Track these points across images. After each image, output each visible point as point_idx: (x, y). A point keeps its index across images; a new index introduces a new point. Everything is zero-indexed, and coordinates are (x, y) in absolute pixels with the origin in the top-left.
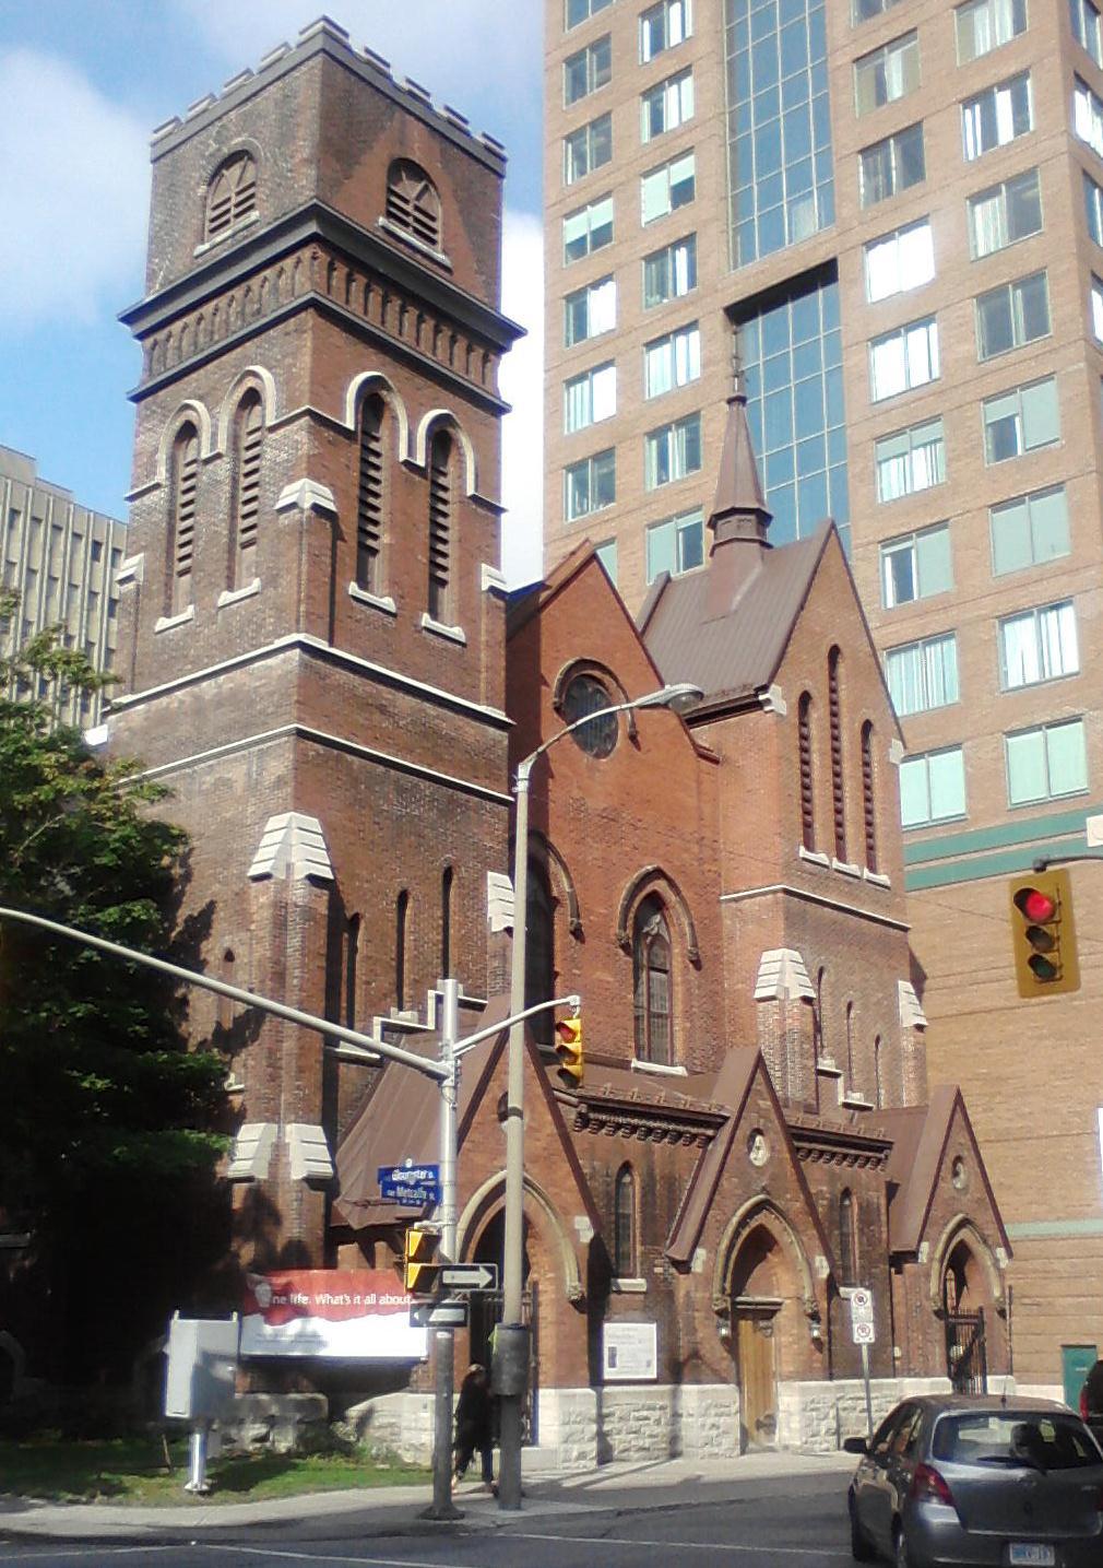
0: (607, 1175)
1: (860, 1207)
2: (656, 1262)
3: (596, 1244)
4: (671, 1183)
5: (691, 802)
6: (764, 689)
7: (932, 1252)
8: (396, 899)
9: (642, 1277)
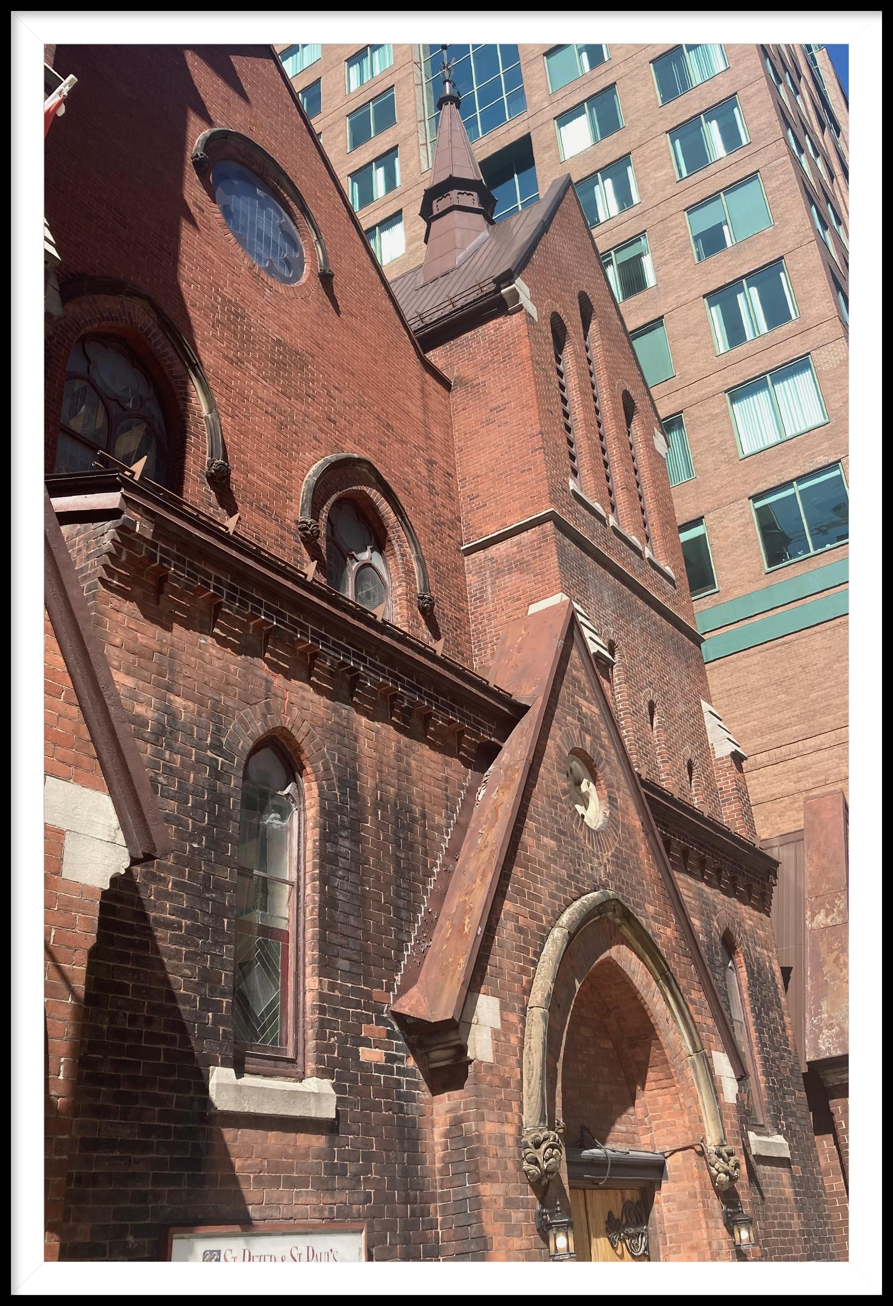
0: (216, 747)
2: (365, 1030)
3: (121, 904)
4: (404, 822)
6: (507, 277)
9: (322, 1074)
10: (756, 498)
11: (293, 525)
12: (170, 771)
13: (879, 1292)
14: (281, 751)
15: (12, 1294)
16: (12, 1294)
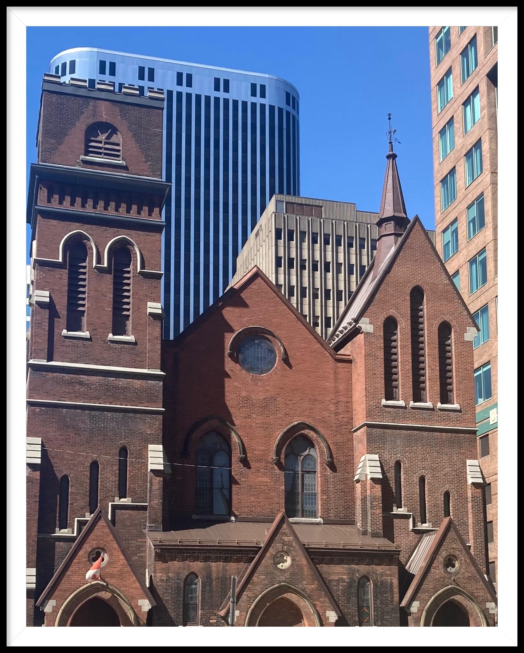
1: (375, 585)
5: (329, 385)
7: (420, 610)
8: (89, 465)
11: (271, 460)
12: (169, 586)
14: (194, 575)
15: (8, 645)
16: (8, 645)
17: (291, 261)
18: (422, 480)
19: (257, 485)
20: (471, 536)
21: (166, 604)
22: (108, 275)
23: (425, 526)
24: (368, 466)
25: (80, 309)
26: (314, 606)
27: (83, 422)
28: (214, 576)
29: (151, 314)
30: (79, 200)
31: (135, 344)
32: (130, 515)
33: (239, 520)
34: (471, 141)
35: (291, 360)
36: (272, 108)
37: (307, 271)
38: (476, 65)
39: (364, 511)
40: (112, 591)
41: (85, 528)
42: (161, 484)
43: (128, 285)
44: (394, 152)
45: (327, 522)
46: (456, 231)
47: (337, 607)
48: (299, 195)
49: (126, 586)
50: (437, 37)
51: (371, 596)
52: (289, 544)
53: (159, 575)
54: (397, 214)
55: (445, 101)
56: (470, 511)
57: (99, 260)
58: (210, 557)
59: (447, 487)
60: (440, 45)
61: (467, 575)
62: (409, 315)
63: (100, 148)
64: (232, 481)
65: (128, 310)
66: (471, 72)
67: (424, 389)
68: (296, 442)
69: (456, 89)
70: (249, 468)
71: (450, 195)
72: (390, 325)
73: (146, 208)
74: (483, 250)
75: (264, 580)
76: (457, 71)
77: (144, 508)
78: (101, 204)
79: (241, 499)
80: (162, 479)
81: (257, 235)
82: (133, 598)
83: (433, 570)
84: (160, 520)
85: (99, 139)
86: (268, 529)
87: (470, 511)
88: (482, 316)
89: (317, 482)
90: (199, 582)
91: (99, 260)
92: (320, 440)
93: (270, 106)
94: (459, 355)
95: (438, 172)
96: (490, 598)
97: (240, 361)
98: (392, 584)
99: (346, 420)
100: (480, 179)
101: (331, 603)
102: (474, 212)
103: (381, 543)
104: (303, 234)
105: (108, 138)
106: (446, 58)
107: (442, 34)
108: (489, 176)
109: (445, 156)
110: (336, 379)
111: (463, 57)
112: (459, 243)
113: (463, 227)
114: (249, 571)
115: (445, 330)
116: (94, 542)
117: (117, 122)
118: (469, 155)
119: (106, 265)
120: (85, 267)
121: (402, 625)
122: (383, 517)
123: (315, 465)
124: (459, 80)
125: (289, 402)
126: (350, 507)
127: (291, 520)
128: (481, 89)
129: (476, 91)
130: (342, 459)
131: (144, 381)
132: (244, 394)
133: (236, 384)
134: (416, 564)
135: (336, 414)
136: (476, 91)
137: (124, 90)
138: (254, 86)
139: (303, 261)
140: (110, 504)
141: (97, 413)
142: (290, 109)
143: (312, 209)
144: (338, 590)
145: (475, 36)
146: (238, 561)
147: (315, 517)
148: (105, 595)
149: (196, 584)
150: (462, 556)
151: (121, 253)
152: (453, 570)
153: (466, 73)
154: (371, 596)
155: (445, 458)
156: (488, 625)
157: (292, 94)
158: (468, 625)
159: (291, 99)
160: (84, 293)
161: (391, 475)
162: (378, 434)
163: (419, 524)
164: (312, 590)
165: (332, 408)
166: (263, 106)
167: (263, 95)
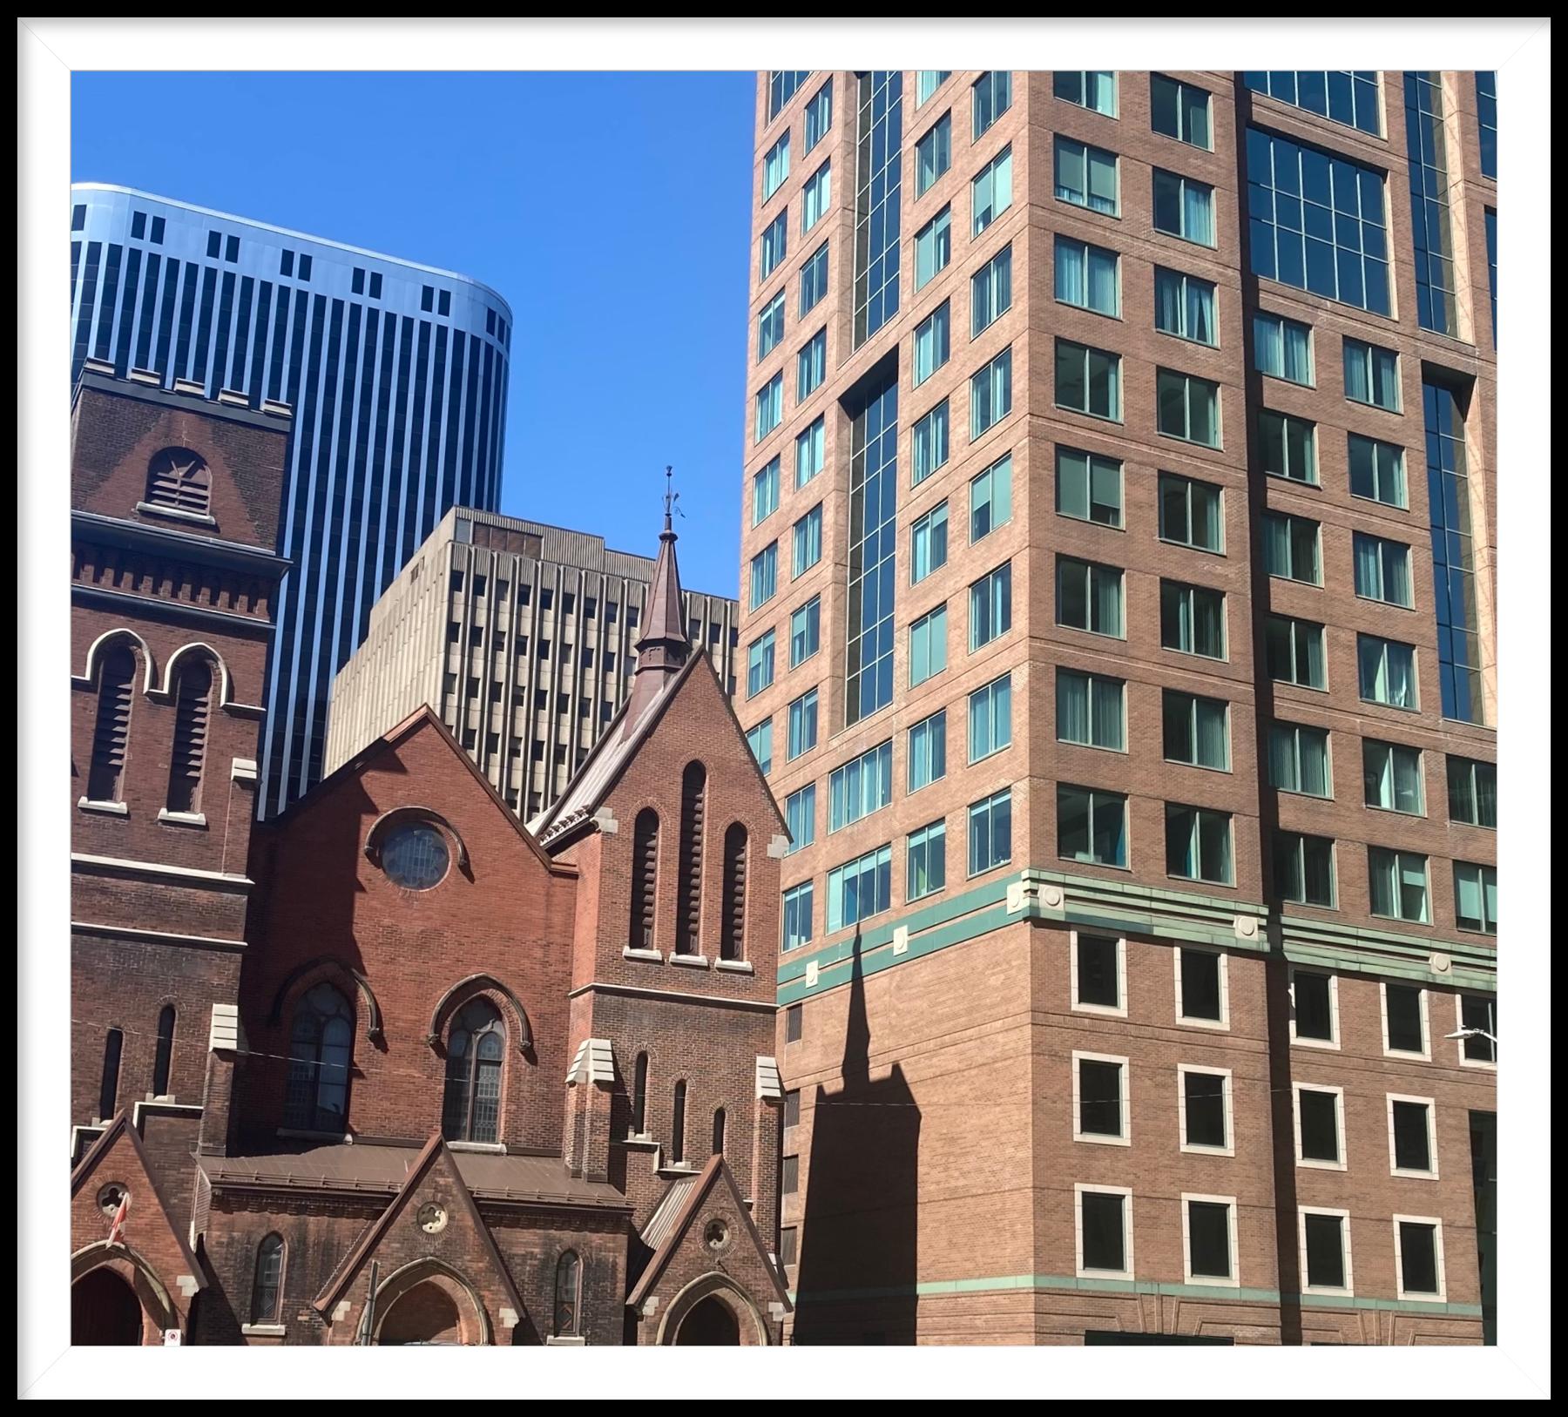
1: (587, 1266)
5: (538, 914)
7: (659, 1312)
10: (972, 806)
13: (1548, 1397)
15: (20, 1397)
16: (20, 1397)
17: (476, 632)
18: (681, 1086)
19: (395, 1080)
20: (755, 1187)
21: (225, 1286)
22: (168, 708)
23: (680, 1167)
24: (590, 1059)
25: (114, 762)
26: (481, 1299)
27: (102, 958)
28: (311, 1239)
29: (237, 779)
30: (128, 577)
31: (206, 828)
32: (171, 1125)
33: (360, 1140)
34: (805, 504)
35: (473, 868)
36: (459, 336)
37: (505, 653)
38: (823, 378)
39: (579, 1135)
40: (135, 1260)
41: (95, 1146)
42: (230, 1073)
43: (202, 726)
44: (674, 531)
45: (513, 1151)
46: (770, 650)
47: (518, 1302)
48: (498, 511)
49: (157, 1251)
50: (762, 312)
51: (577, 1284)
52: (446, 1190)
53: (215, 1233)
54: (671, 636)
55: (768, 424)
56: (756, 1143)
57: (156, 681)
58: (307, 1207)
59: (722, 1101)
60: (766, 326)
61: (741, 1254)
62: (679, 808)
63: (174, 491)
64: (353, 1073)
65: (198, 769)
66: (813, 387)
67: (695, 933)
68: (471, 1007)
69: (789, 409)
70: (385, 1050)
71: (767, 586)
72: (646, 822)
73: (244, 599)
74: (813, 690)
75: (398, 1250)
76: (791, 380)
77: (196, 1115)
78: (167, 585)
79: (366, 1106)
80: (231, 1065)
81: (415, 574)
82: (168, 1272)
83: (685, 1244)
84: (223, 1137)
85: (172, 475)
86: (411, 1162)
87: (756, 1143)
88: (805, 799)
89: (501, 1083)
90: (285, 1248)
91: (156, 681)
92: (512, 1008)
93: (456, 331)
94: (757, 878)
95: (749, 542)
96: (775, 1295)
97: (385, 864)
98: (615, 1264)
99: (560, 975)
100: (814, 571)
101: (510, 1294)
102: (802, 622)
103: (601, 1194)
104: (502, 584)
105: (189, 474)
106: (775, 353)
107: (771, 311)
108: (831, 568)
109: (762, 515)
110: (549, 905)
111: (802, 358)
112: (776, 670)
113: (783, 645)
114: (372, 1233)
115: (736, 836)
116: (109, 1173)
117: (206, 449)
118: (800, 524)
119: (166, 691)
120: (128, 692)
121: (625, 1343)
122: (610, 1148)
123: (500, 1050)
124: (792, 396)
125: (464, 940)
126: (556, 1128)
127: (451, 1144)
128: (827, 418)
129: (819, 420)
130: (548, 1042)
131: (215, 894)
132: (387, 921)
133: (374, 903)
134: (659, 1232)
135: (545, 964)
136: (819, 420)
137: (221, 397)
138: (428, 292)
139: (499, 635)
140: (137, 1104)
141: (129, 945)
142: (493, 340)
143: (524, 539)
144: (524, 1272)
145: (825, 327)
146: (355, 1215)
147: (493, 1141)
148: (126, 1268)
149: (279, 1252)
150: (736, 1223)
151: (195, 672)
152: (719, 1245)
153: (806, 387)
154: (577, 1284)
155: (722, 1051)
156: (770, 1343)
157: (500, 313)
158: (737, 1343)
159: (497, 322)
160: (123, 735)
161: (630, 1076)
162: (613, 1004)
163: (670, 1162)
164: (480, 1271)
165: (538, 953)
166: (442, 330)
167: (444, 310)
